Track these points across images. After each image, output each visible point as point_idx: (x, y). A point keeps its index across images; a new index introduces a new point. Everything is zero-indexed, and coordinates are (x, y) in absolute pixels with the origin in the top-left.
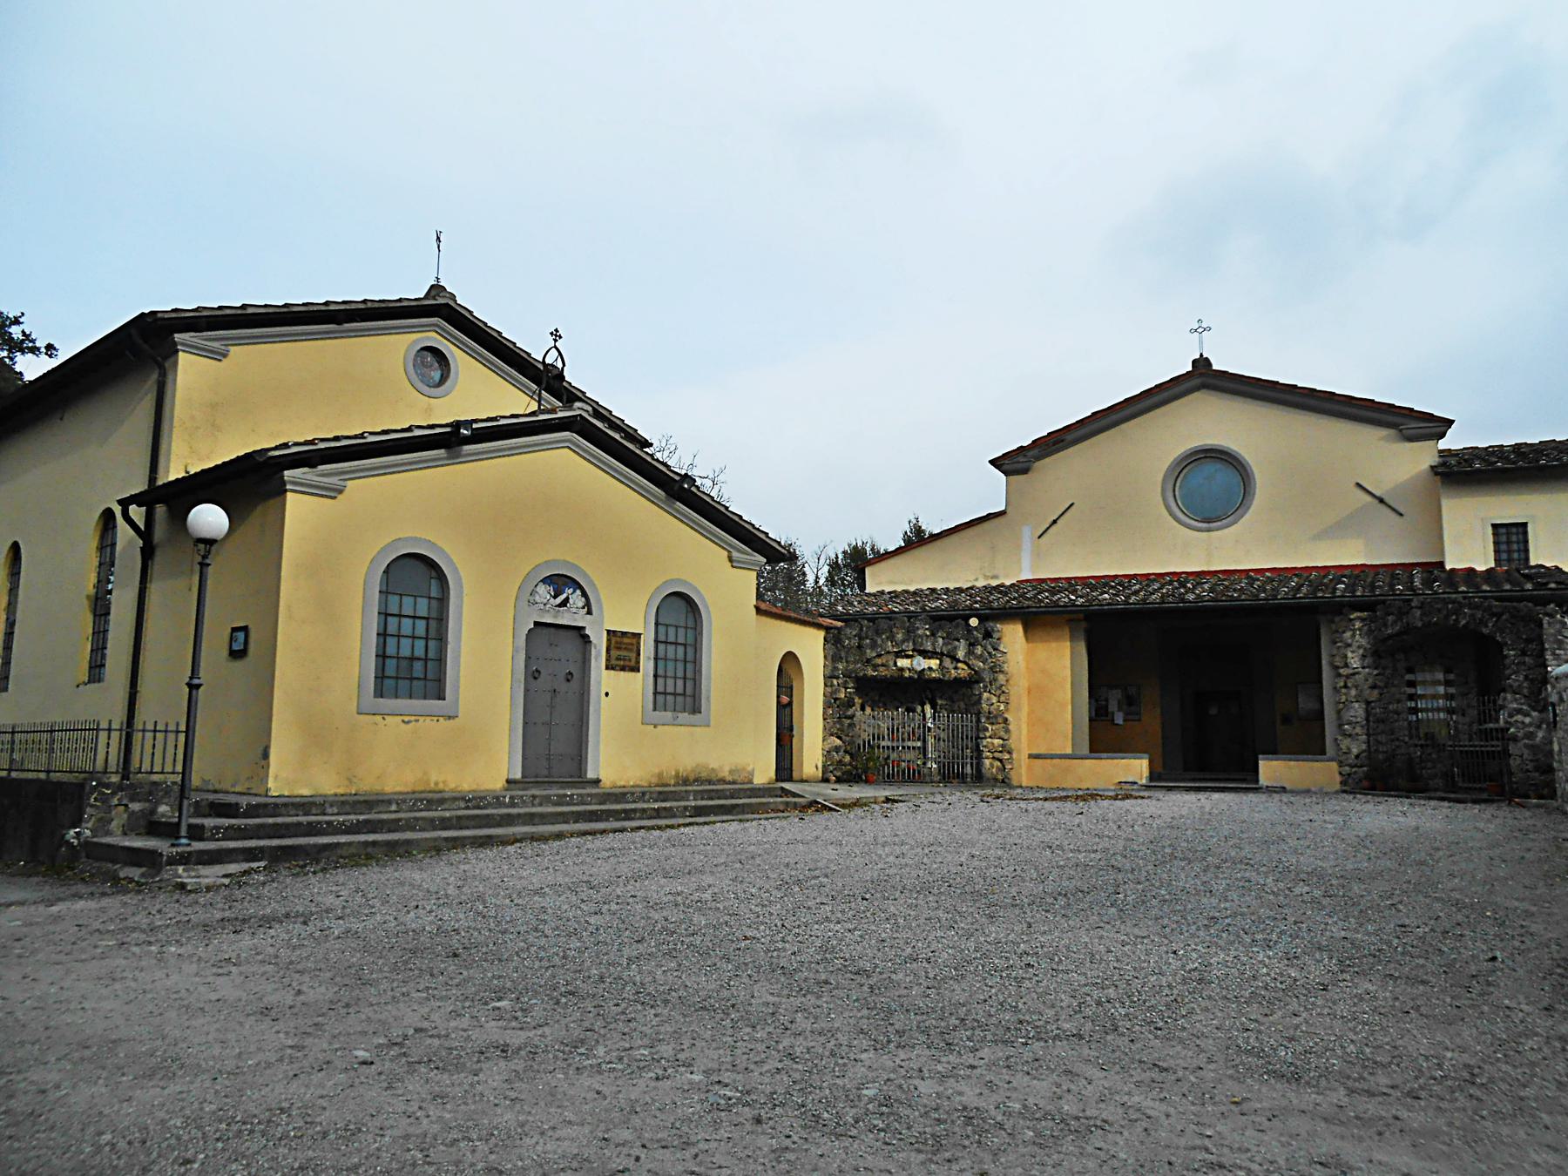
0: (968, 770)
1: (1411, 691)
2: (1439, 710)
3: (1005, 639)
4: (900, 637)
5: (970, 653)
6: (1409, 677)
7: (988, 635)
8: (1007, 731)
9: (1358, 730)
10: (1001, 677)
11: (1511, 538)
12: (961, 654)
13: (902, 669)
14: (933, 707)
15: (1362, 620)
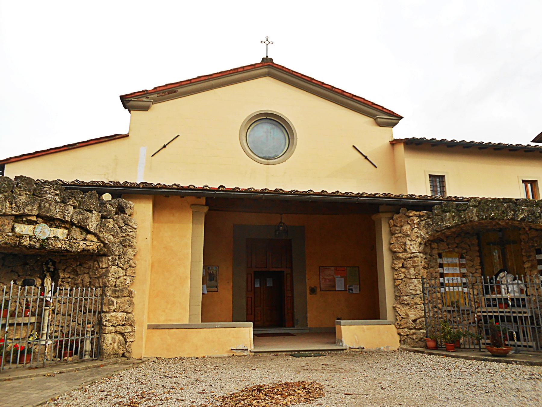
0: (88, 347)
1: (440, 270)
2: (457, 285)
3: (134, 216)
4: (23, 199)
5: (102, 225)
6: (439, 261)
7: (121, 210)
8: (131, 304)
9: (418, 300)
10: (130, 251)
11: (437, 181)
12: (92, 225)
13: (21, 236)
14: (55, 278)
15: (420, 216)
